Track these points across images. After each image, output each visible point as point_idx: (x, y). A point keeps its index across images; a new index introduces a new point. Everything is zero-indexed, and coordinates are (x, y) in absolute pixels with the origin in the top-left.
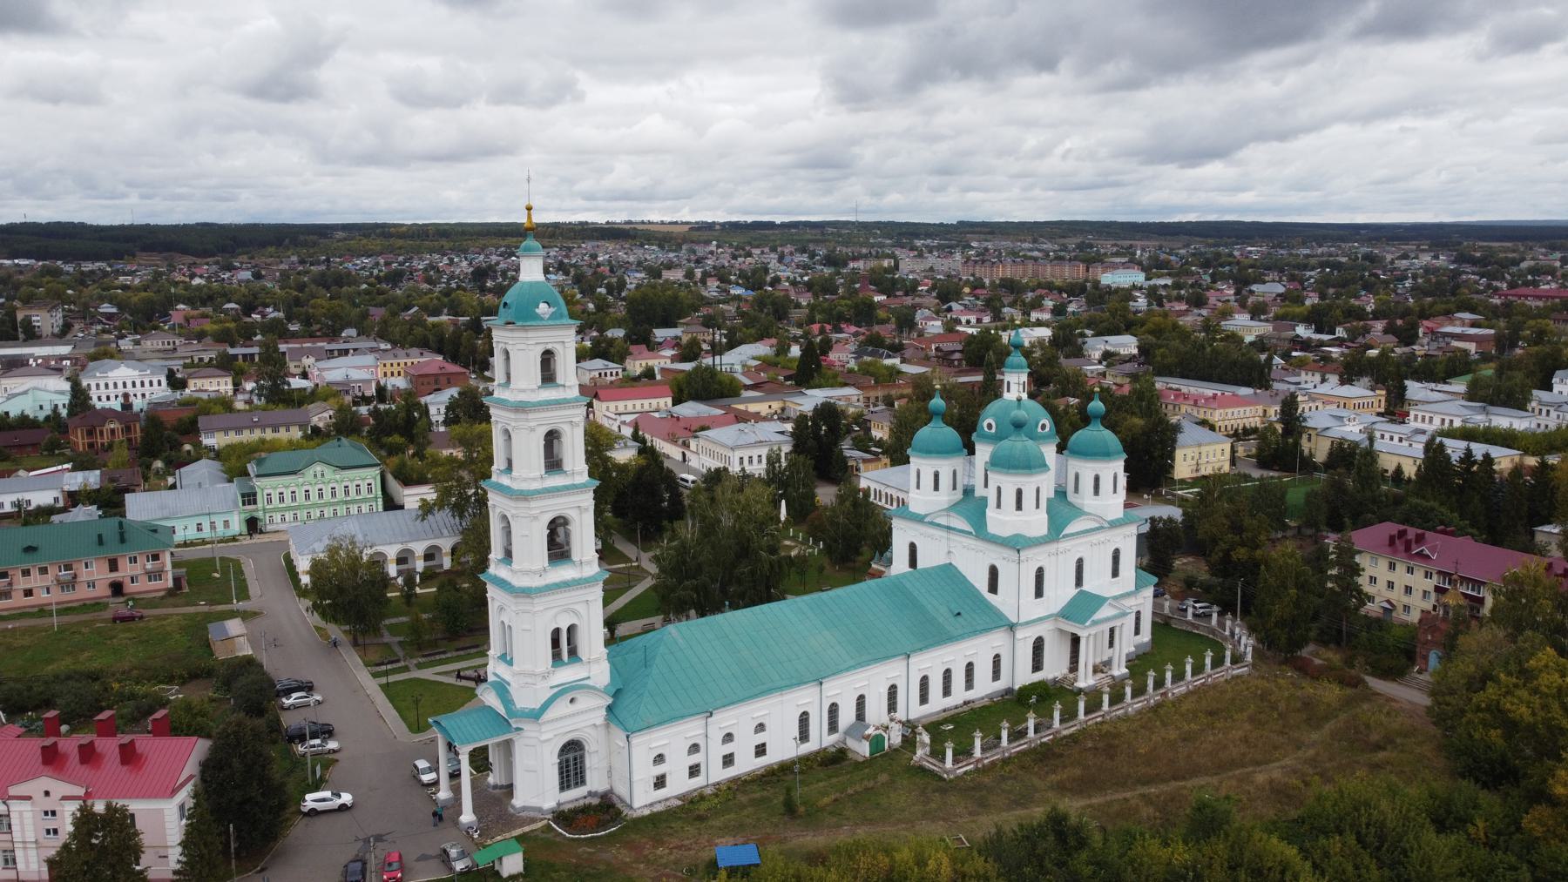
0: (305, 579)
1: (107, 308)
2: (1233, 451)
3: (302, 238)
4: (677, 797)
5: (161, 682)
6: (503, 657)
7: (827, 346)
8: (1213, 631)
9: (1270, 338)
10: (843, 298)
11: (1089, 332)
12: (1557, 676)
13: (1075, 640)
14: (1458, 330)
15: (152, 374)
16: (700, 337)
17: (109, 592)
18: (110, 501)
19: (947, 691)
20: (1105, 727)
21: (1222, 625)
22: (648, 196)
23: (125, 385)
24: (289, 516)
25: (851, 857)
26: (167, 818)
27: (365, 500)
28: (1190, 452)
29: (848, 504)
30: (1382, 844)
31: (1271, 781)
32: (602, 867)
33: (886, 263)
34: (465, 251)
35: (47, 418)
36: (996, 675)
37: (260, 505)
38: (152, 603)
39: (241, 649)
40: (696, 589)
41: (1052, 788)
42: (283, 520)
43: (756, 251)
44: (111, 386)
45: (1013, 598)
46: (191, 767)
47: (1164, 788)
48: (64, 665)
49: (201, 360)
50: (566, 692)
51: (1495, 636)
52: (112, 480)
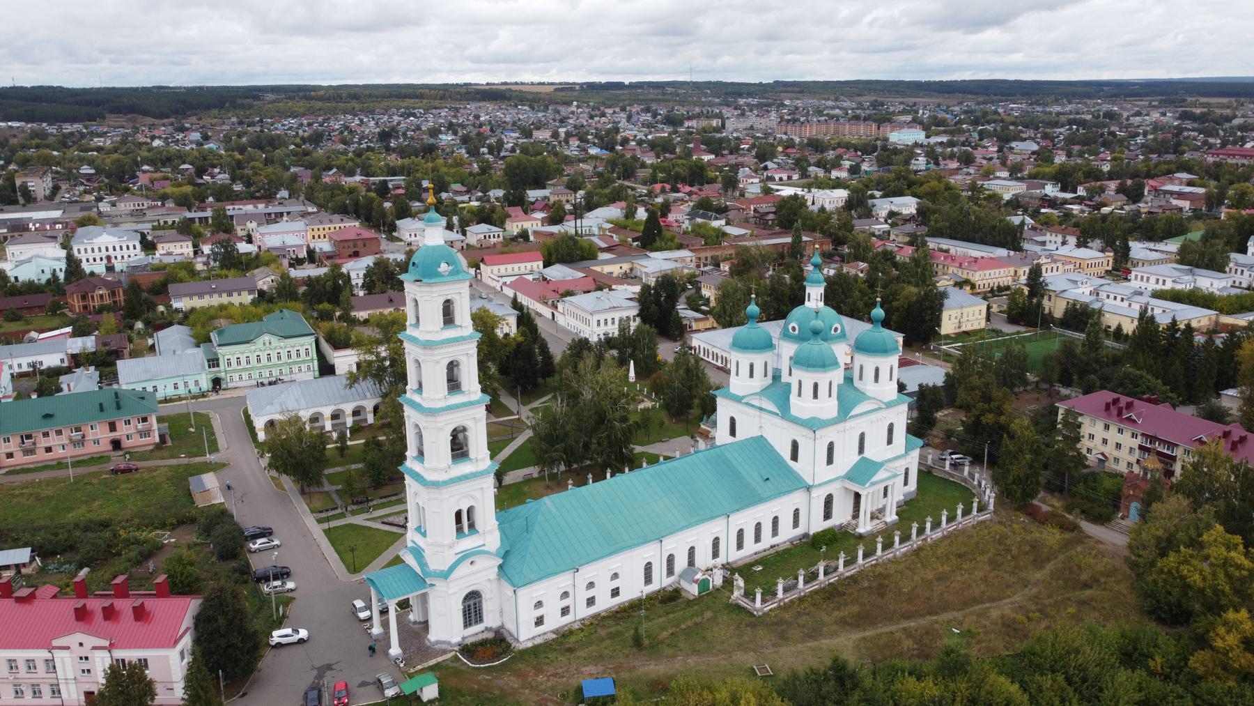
0: (261, 436)
1: (86, 170)
2: (989, 308)
3: (240, 101)
4: (553, 632)
5: (157, 528)
6: (418, 529)
7: (666, 208)
8: (965, 480)
9: (1023, 196)
10: (680, 158)
11: (878, 194)
12: (1223, 549)
13: (857, 496)
14: (1176, 188)
15: (129, 239)
16: (564, 199)
17: (110, 448)
18: (105, 362)
19: (758, 539)
20: (879, 569)
21: (972, 476)
22: (524, 59)
23: (107, 249)
24: (245, 375)
25: (683, 696)
26: (172, 667)
27: (304, 362)
28: (954, 313)
29: (681, 372)
30: (1086, 685)
31: (1003, 616)
32: (497, 692)
33: (715, 123)
34: (372, 112)
35: (48, 281)
36: (796, 523)
37: (222, 367)
38: (143, 456)
39: (215, 498)
40: (565, 451)
41: (836, 623)
42: (241, 378)
43: (610, 111)
44: (96, 250)
45: (810, 466)
46: (188, 622)
47: (923, 622)
48: (79, 514)
49: (166, 222)
50: (467, 556)
51: (1180, 504)
52: (105, 344)
